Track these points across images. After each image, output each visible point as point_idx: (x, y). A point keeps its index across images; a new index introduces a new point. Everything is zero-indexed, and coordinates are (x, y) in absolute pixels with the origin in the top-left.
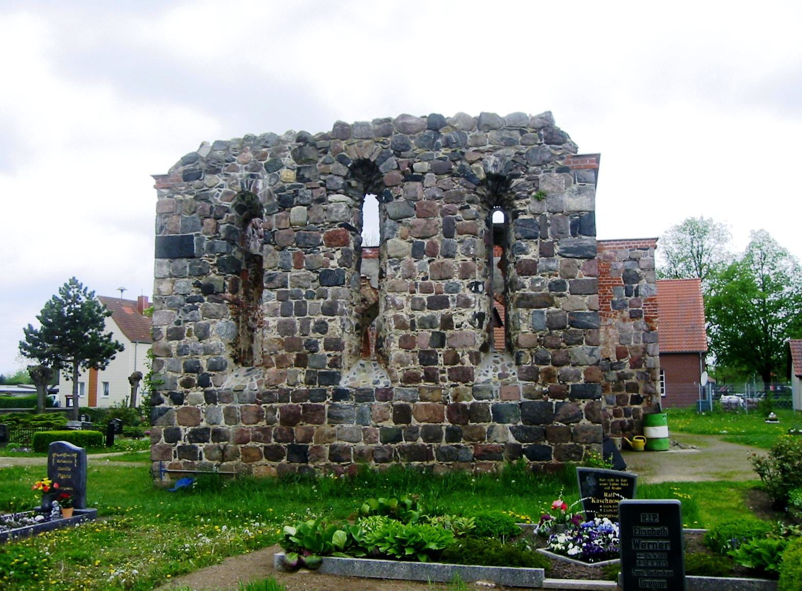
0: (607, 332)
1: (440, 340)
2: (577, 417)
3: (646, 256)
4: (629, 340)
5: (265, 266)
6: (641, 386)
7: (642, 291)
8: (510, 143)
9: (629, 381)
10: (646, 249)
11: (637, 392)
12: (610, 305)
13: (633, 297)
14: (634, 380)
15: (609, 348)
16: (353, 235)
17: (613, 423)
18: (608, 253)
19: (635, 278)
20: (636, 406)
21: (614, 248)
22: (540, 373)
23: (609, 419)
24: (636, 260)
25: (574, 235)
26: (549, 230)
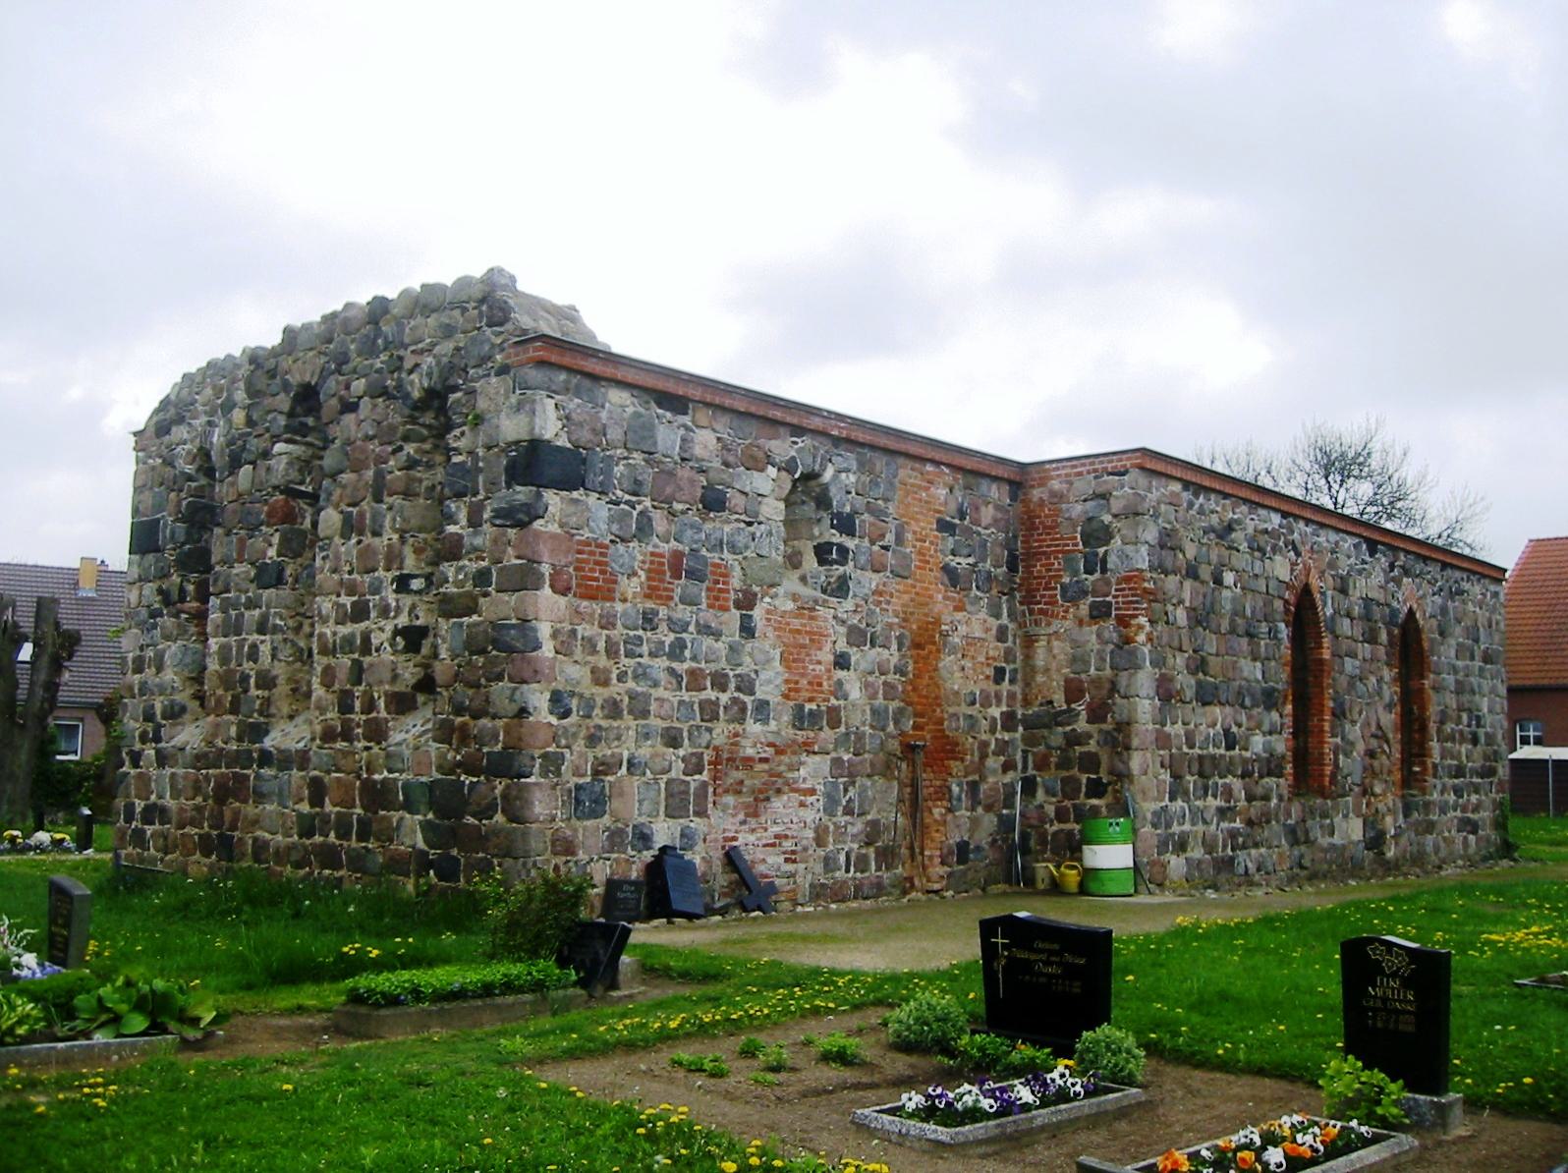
0: (1050, 649)
1: (358, 672)
2: (487, 812)
3: (1122, 487)
4: (1087, 663)
5: (214, 560)
6: (1104, 759)
7: (1113, 561)
8: (448, 331)
9: (1085, 749)
10: (1123, 474)
11: (1097, 773)
12: (1058, 592)
13: (1097, 575)
14: (1092, 746)
15: (1052, 680)
16: (310, 505)
17: (1055, 834)
18: (1056, 485)
19: (1101, 535)
20: (1095, 802)
21: (1067, 475)
22: (340, 734)
23: (1047, 826)
24: (1104, 496)
25: (509, 486)
26: (481, 479)
